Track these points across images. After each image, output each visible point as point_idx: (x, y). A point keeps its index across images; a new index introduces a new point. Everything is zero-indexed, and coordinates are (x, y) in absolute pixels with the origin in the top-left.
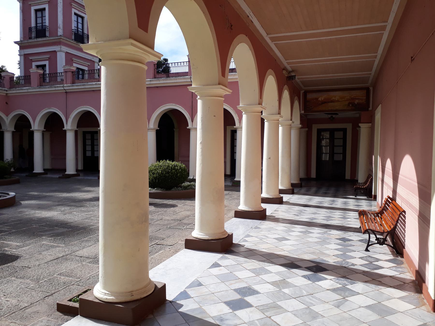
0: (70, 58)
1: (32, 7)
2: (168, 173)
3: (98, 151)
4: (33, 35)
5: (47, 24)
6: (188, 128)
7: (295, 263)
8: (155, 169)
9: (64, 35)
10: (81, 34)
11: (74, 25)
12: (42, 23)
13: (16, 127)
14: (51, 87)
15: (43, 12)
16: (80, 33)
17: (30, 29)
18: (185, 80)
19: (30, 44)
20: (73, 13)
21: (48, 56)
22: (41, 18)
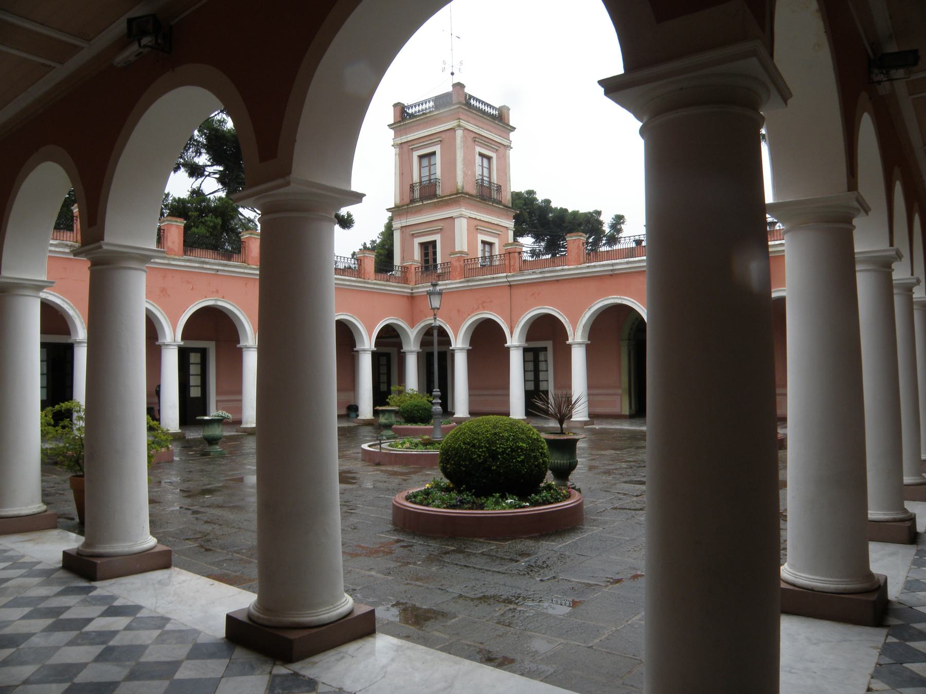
0: (476, 226)
1: (214, 343)
6: (506, 345)
11: (478, 171)
13: (423, 344)
15: (432, 158)
16: (486, 184)
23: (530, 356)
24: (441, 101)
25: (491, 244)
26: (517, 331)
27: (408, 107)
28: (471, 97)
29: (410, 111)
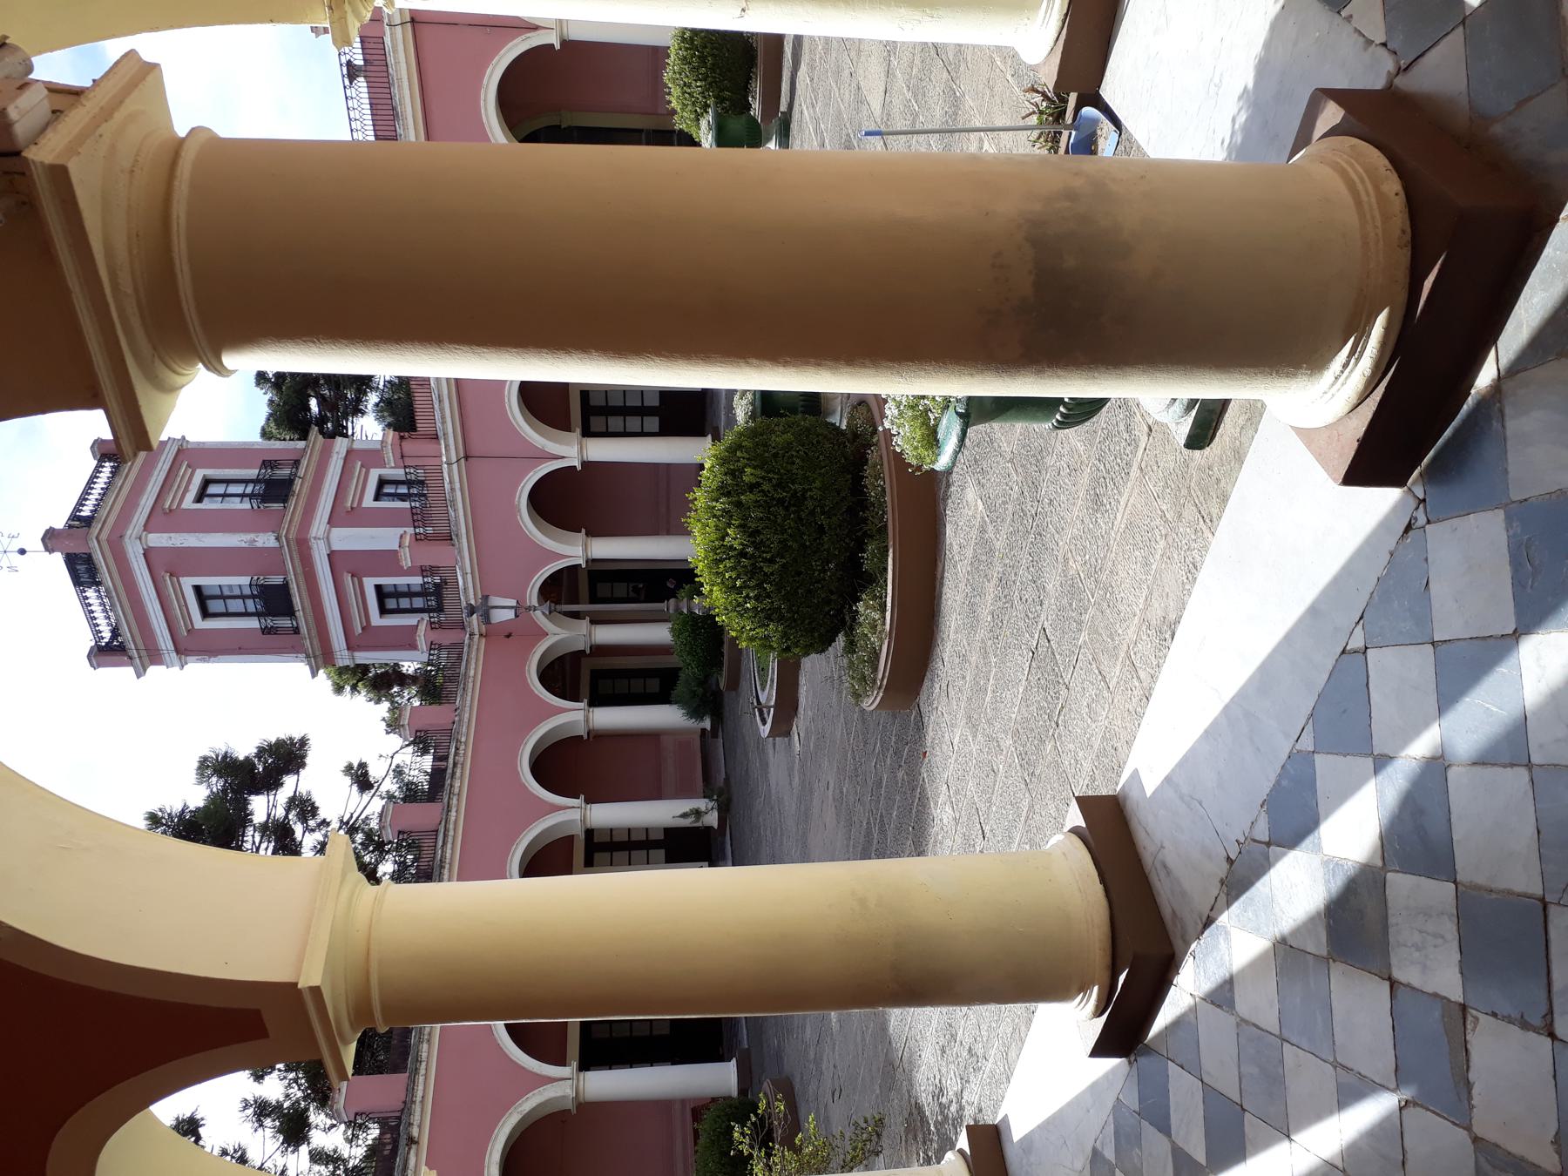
2: (702, 59)
3: (642, 392)
4: (285, 622)
5: (244, 581)
6: (557, 47)
7: (1493, 352)
8: (694, 104)
9: (276, 530)
10: (259, 488)
12: (243, 597)
14: (453, 502)
15: (206, 592)
16: (259, 488)
17: (266, 631)
18: (401, 47)
19: (314, 632)
20: (198, 506)
21: (348, 579)
22: (229, 601)
23: (597, 423)
24: (82, 571)
25: (382, 483)
26: (552, 447)
27: (97, 633)
28: (74, 516)
29: (107, 635)
